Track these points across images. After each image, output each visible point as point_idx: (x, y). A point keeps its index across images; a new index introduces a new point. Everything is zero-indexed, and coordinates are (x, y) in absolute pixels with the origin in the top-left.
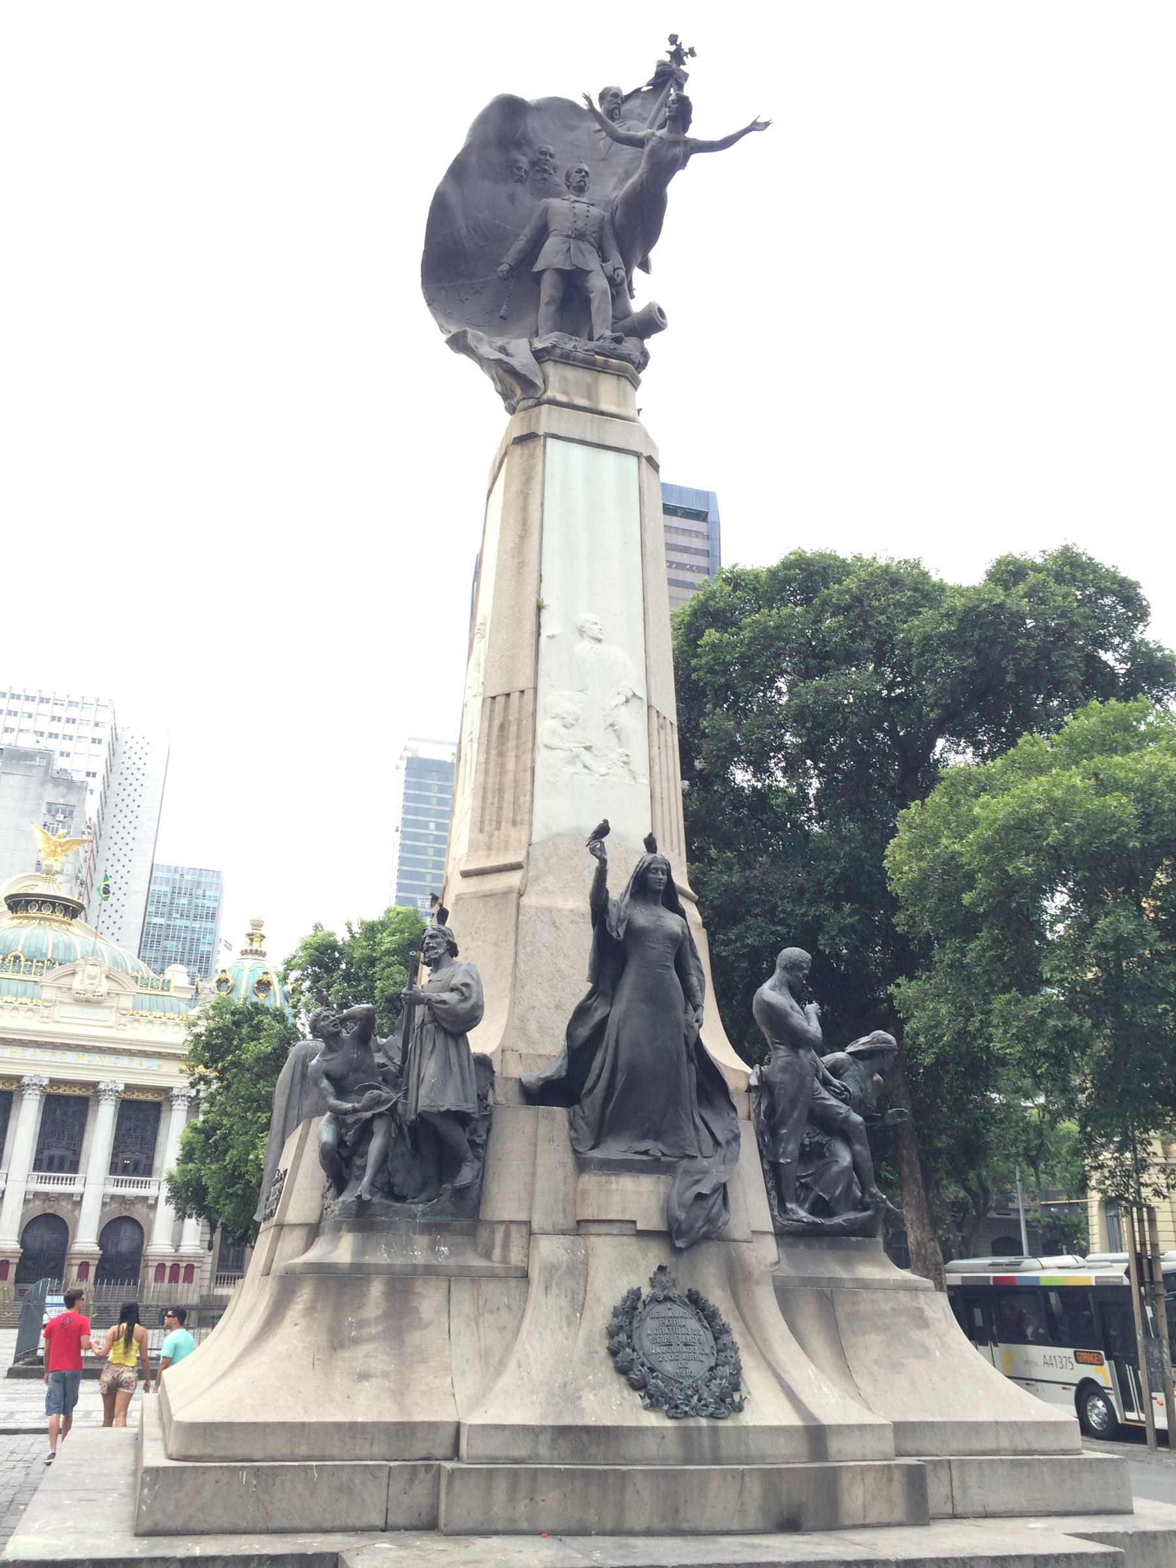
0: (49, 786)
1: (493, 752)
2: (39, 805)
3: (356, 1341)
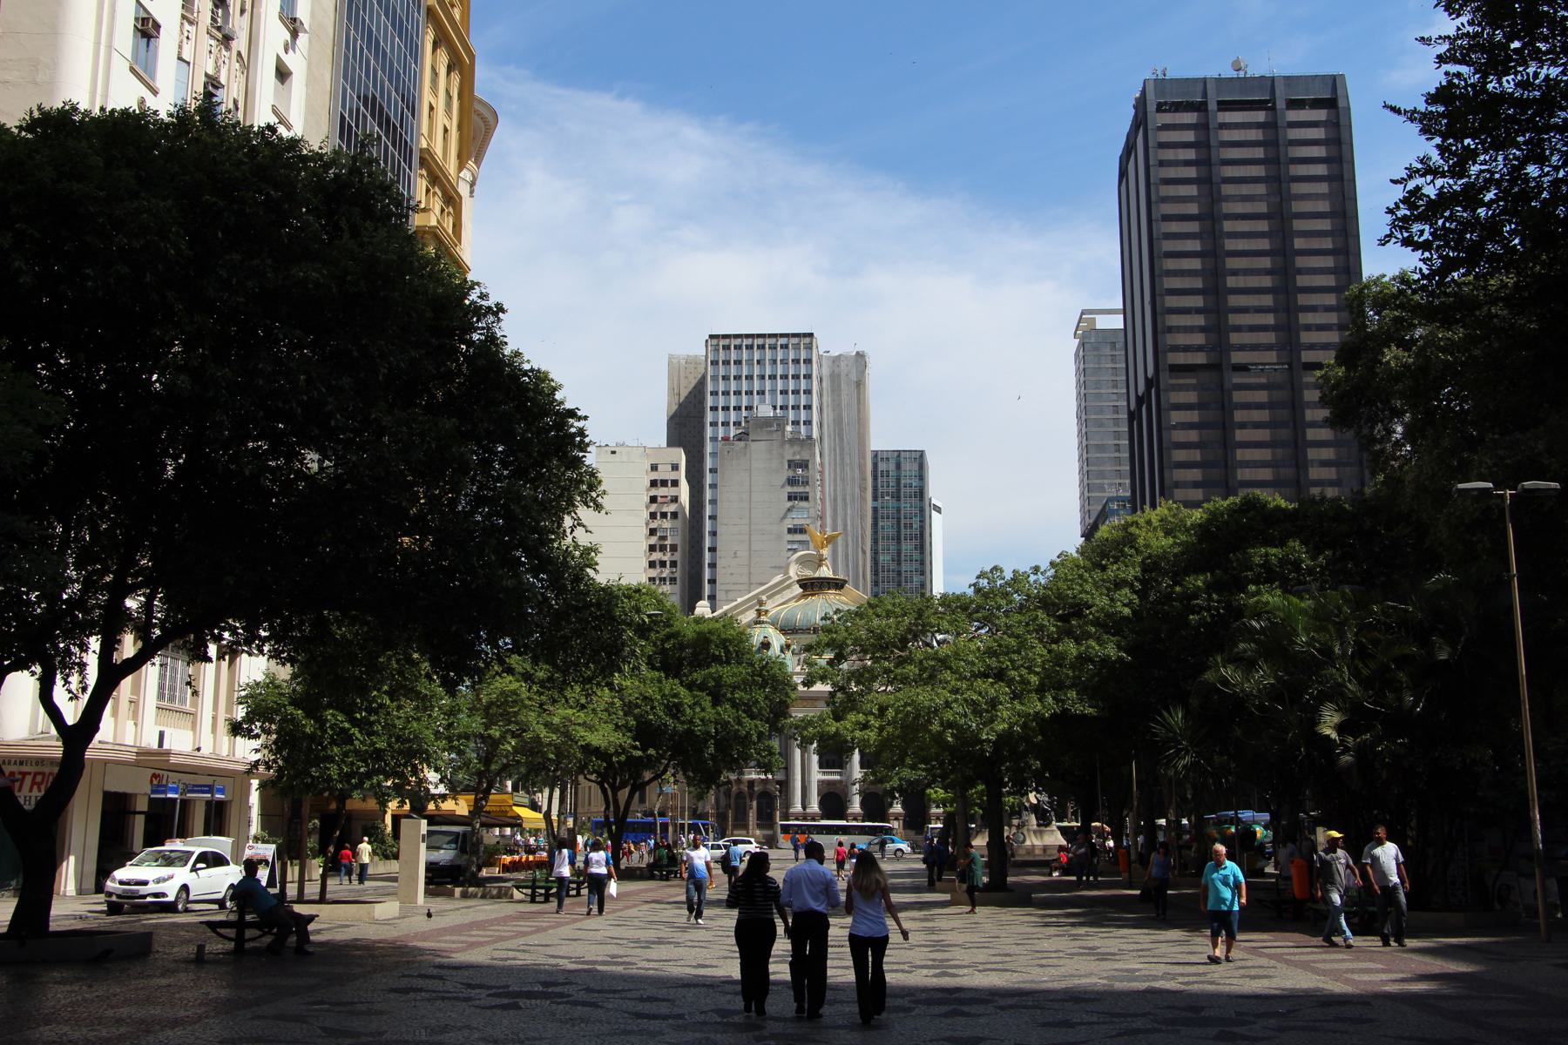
0: (787, 446)
2: (782, 463)
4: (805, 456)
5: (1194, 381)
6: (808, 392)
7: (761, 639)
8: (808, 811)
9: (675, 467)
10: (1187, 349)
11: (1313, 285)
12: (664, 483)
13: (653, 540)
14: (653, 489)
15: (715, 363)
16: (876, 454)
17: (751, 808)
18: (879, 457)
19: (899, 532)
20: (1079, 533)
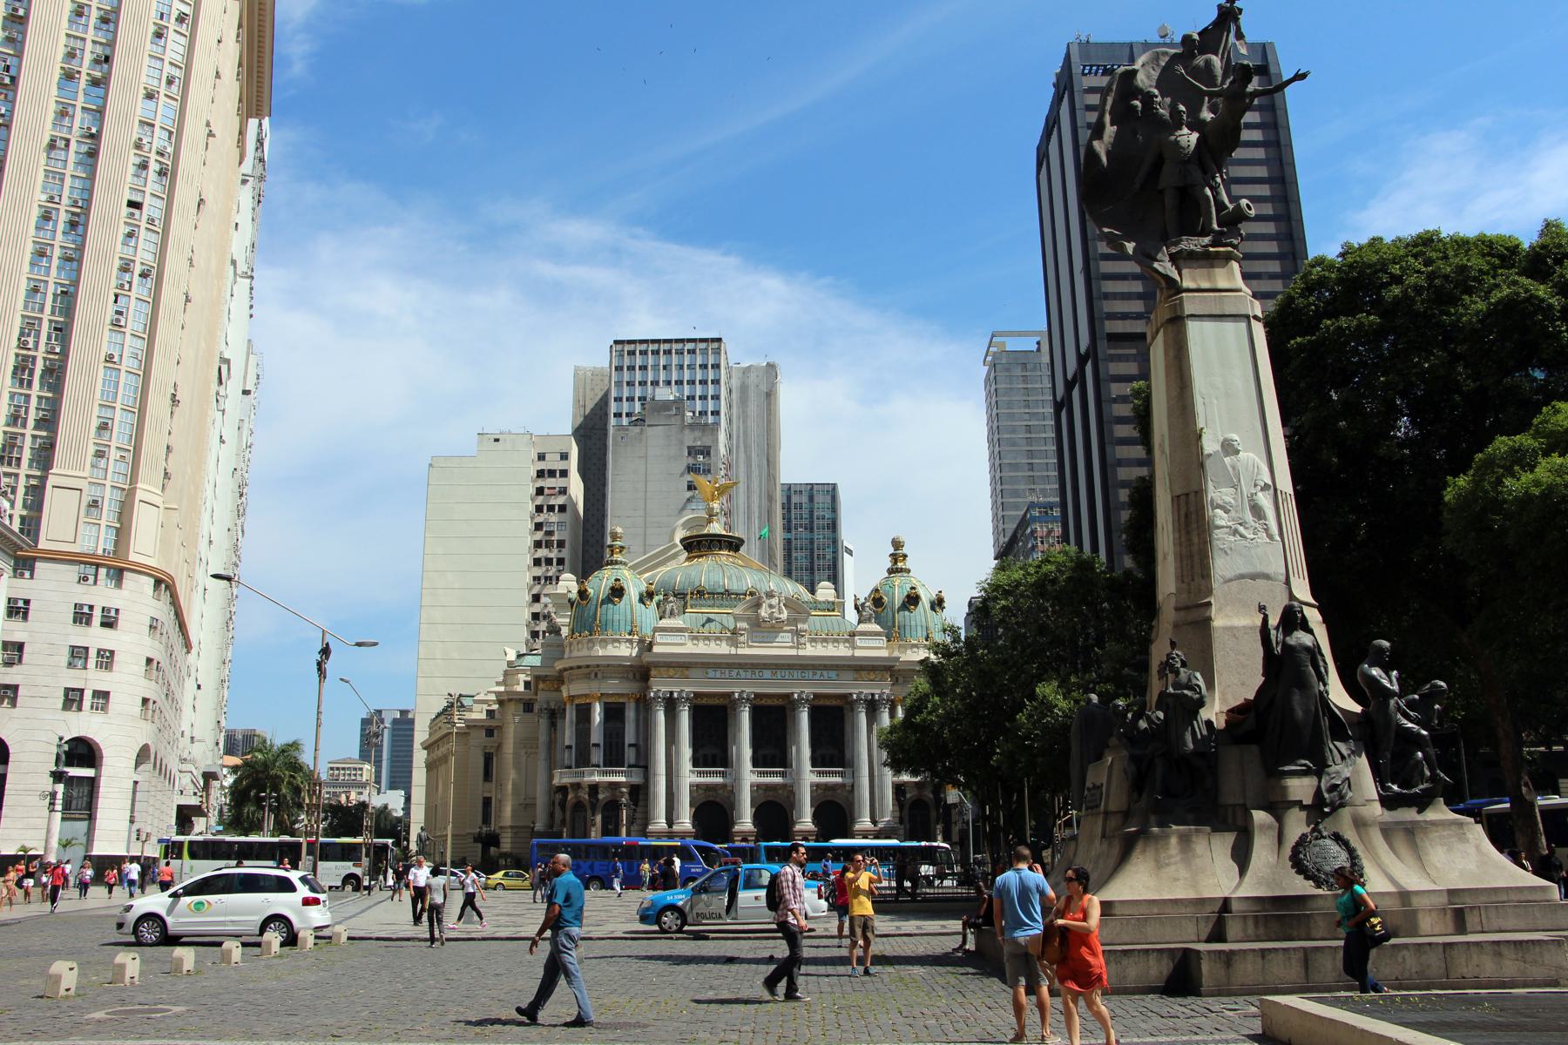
0: (687, 432)
1: (1183, 532)
2: (681, 449)
3: (1168, 865)
4: (707, 441)
5: (1134, 351)
6: (716, 397)
7: (611, 582)
8: (676, 828)
9: (565, 456)
10: (1125, 316)
11: (1256, 251)
12: (552, 473)
13: (539, 535)
14: (540, 480)
15: (619, 369)
16: (789, 490)
17: (594, 825)
18: (792, 490)
19: (812, 563)
20: (993, 555)
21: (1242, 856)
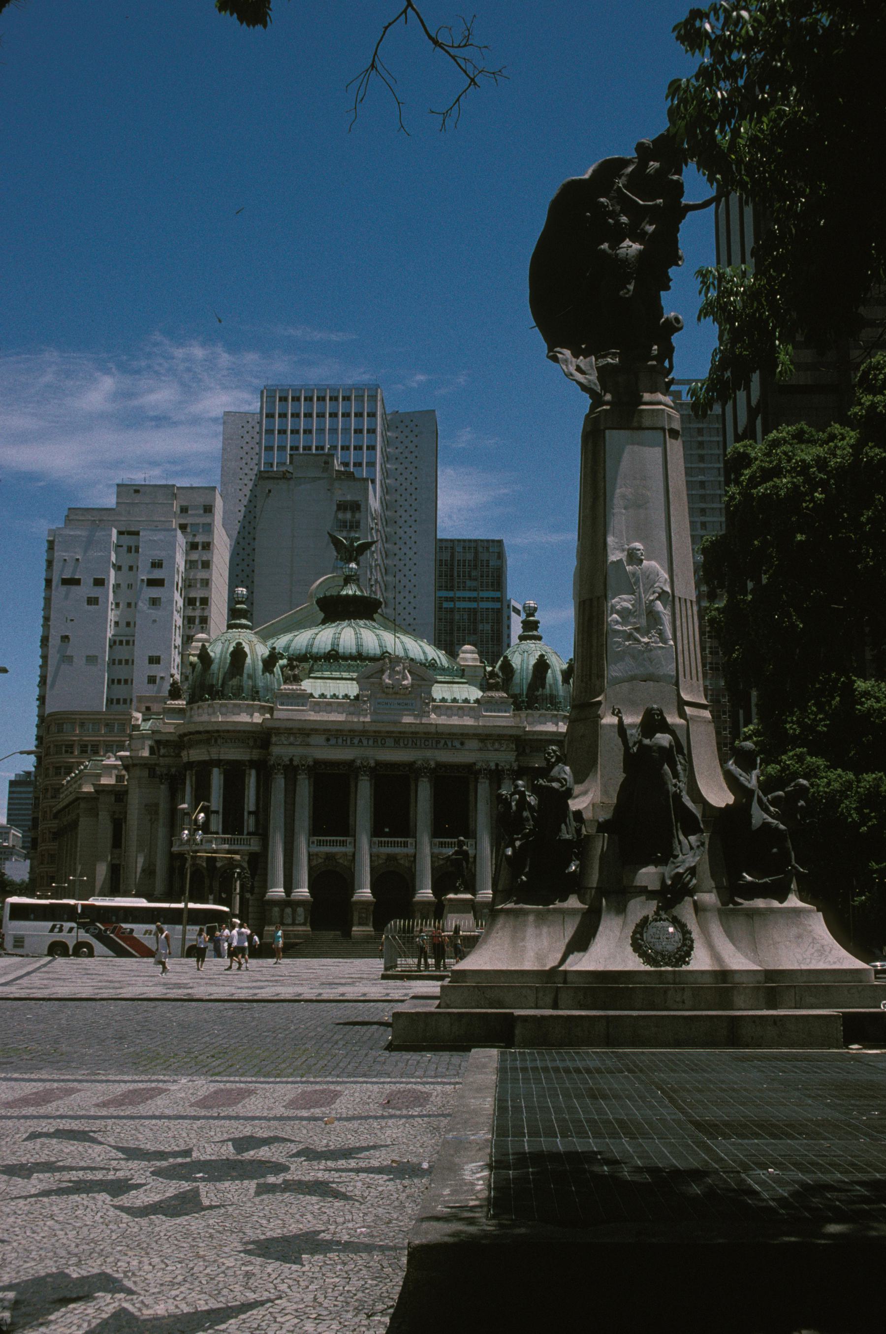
21: (457, 930)
